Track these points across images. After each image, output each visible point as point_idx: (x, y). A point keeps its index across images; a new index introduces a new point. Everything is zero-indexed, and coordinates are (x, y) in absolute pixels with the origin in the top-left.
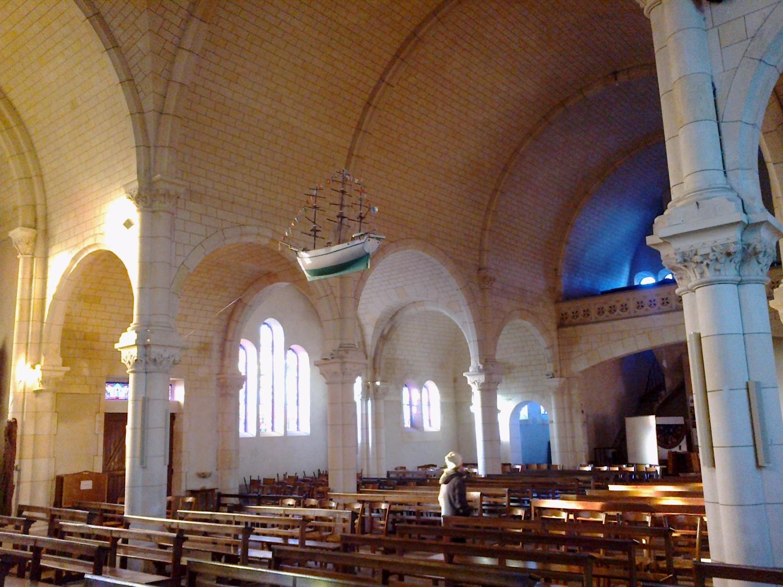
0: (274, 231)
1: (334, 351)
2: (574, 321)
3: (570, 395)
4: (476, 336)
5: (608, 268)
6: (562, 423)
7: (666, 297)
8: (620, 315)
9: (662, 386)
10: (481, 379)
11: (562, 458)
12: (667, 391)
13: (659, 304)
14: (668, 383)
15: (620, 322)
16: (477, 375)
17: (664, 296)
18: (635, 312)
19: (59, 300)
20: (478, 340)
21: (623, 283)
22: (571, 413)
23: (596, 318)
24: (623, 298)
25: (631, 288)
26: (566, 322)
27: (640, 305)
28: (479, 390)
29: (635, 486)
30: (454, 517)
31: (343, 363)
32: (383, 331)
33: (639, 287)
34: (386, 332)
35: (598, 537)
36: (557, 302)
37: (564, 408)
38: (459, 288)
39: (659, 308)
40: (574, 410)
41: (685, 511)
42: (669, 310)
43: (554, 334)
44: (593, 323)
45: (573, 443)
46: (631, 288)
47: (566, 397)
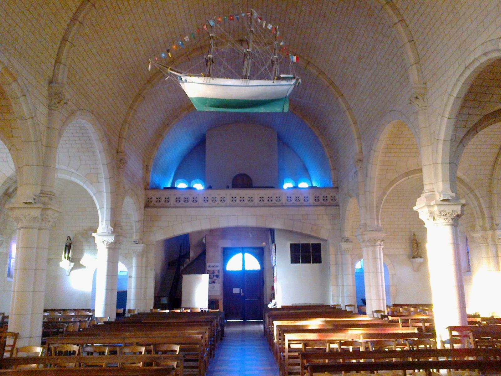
0: (9, 61)
1: (35, 196)
2: (157, 204)
3: (147, 257)
4: (110, 205)
5: (165, 174)
6: (139, 278)
7: (263, 196)
8: (191, 204)
9: (187, 255)
10: (110, 239)
11: (136, 305)
12: (190, 259)
13: (293, 201)
14: (192, 254)
15: (191, 209)
16: (110, 235)
17: (270, 196)
18: (202, 204)
19: (184, 7)
20: (111, 208)
21: (169, 186)
22: (146, 270)
23: (174, 204)
24: (167, 193)
25: (173, 188)
26: (152, 204)
27: (178, 200)
28: (107, 248)
29: (293, 321)
30: (109, 356)
31: (45, 209)
32: (9, 188)
33: (176, 188)
34: (11, 190)
35: (386, 362)
36: (146, 189)
37: (142, 267)
38: (105, 163)
39: (218, 204)
40: (149, 269)
41: (376, 338)
42: (252, 205)
43: (143, 211)
44: (172, 207)
45: (145, 293)
46: (173, 188)
47: (144, 259)
